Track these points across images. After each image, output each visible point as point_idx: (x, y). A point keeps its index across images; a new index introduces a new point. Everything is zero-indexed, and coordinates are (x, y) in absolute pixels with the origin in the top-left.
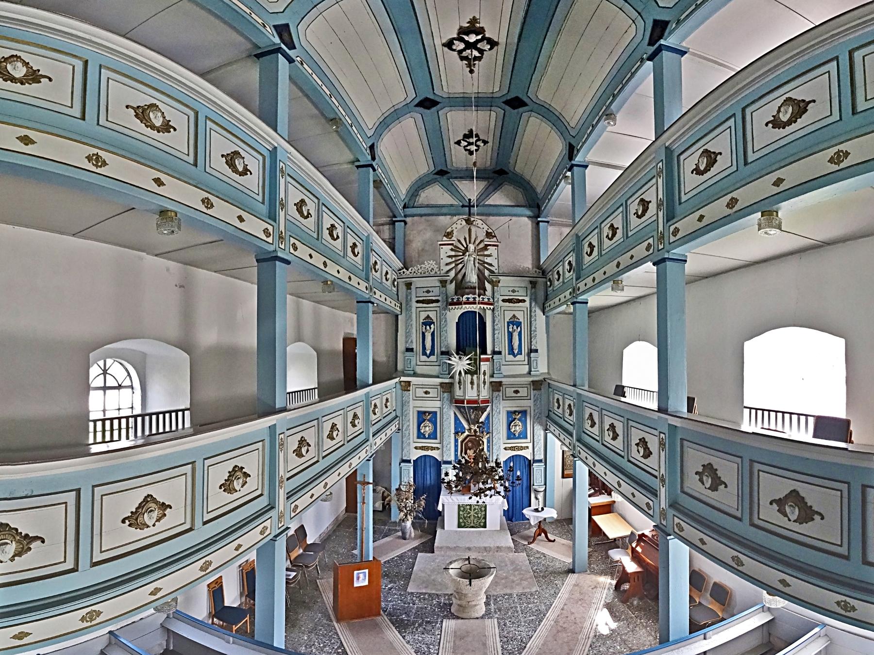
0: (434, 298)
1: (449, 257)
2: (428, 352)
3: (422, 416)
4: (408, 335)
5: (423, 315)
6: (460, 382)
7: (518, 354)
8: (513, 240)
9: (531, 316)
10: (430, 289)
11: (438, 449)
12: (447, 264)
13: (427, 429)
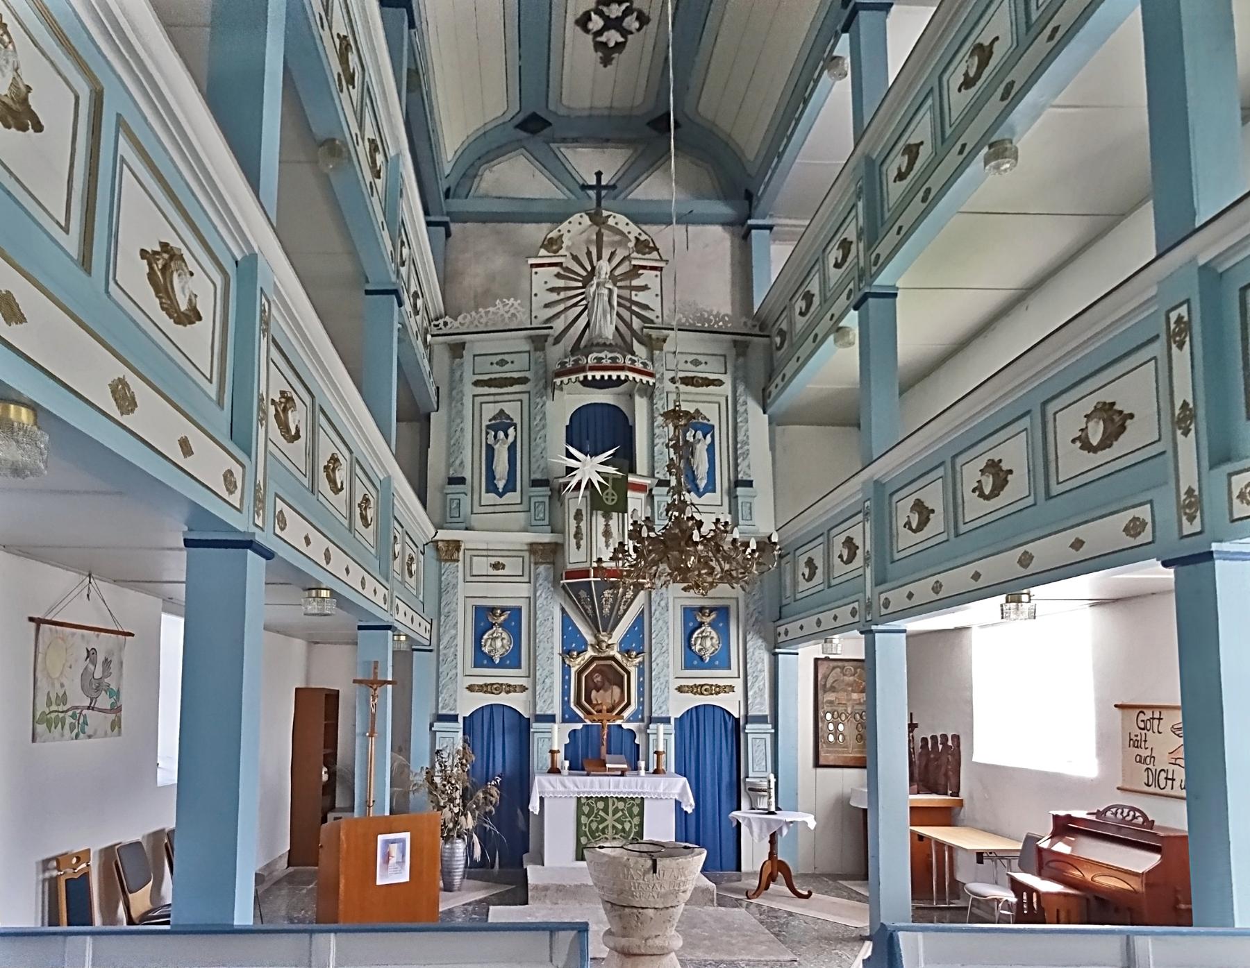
0: (516, 375)
1: (552, 290)
2: (501, 485)
3: (484, 617)
4: (453, 449)
5: (490, 411)
6: (578, 535)
7: (706, 490)
8: (697, 270)
9: (735, 411)
10: (506, 357)
11: (523, 689)
12: (546, 306)
13: (498, 643)
